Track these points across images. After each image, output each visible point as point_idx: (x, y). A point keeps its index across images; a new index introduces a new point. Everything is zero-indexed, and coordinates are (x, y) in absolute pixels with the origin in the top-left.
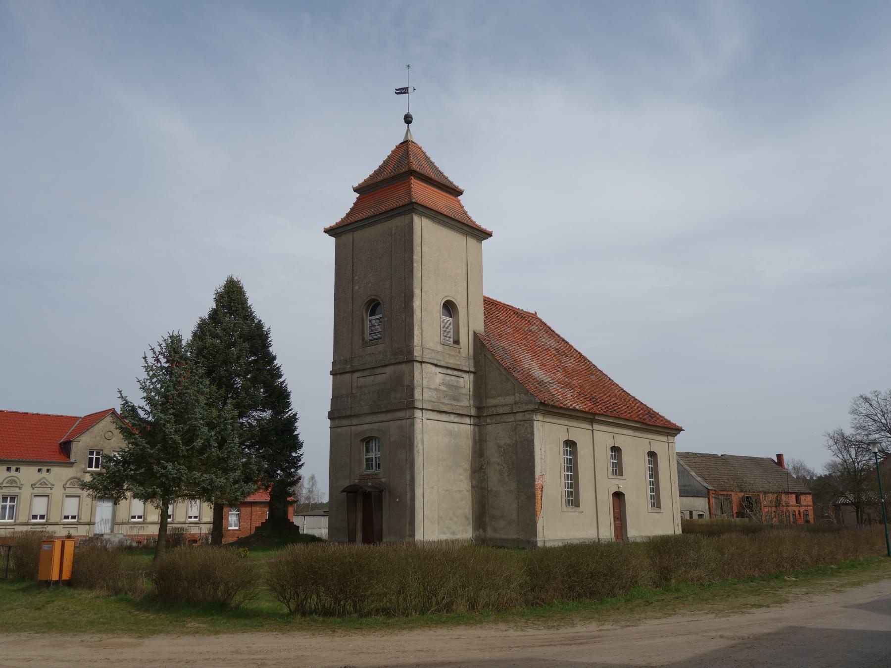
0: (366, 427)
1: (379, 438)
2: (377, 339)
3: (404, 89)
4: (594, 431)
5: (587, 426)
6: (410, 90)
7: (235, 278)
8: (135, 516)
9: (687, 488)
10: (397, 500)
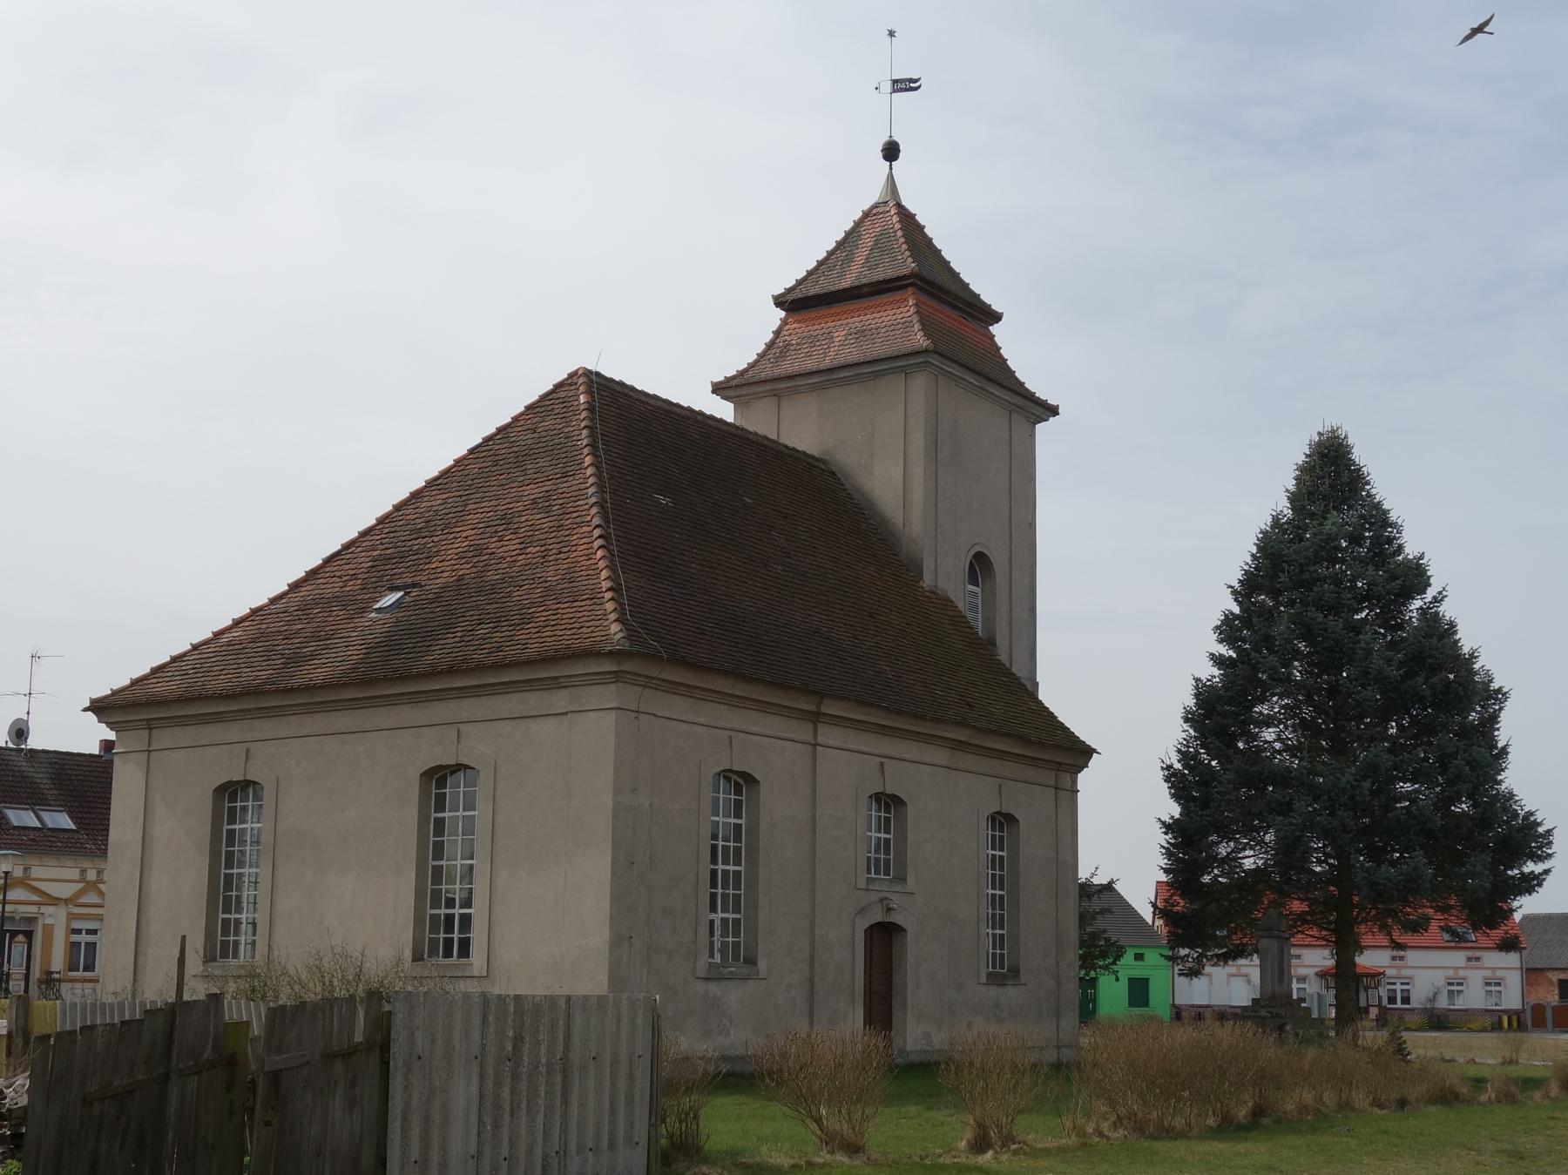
3: (901, 90)
4: (818, 747)
5: (803, 731)
6: (887, 87)
8: (81, 930)
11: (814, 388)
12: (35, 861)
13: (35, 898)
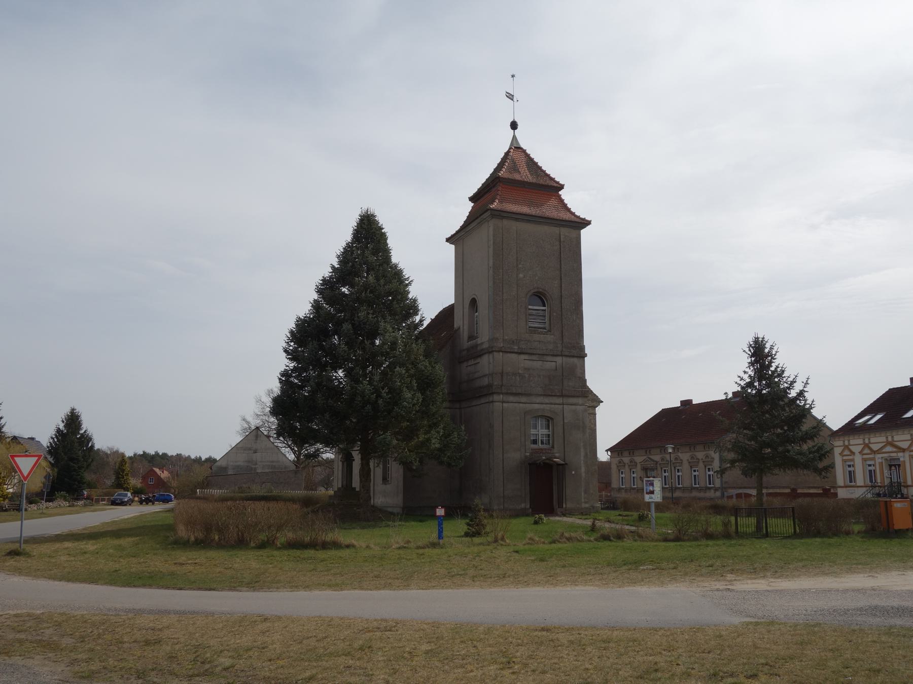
0: (536, 406)
1: (552, 419)
2: (535, 328)
7: (371, 211)
9: (274, 464)
10: (573, 472)
12: (894, 433)
13: (895, 450)
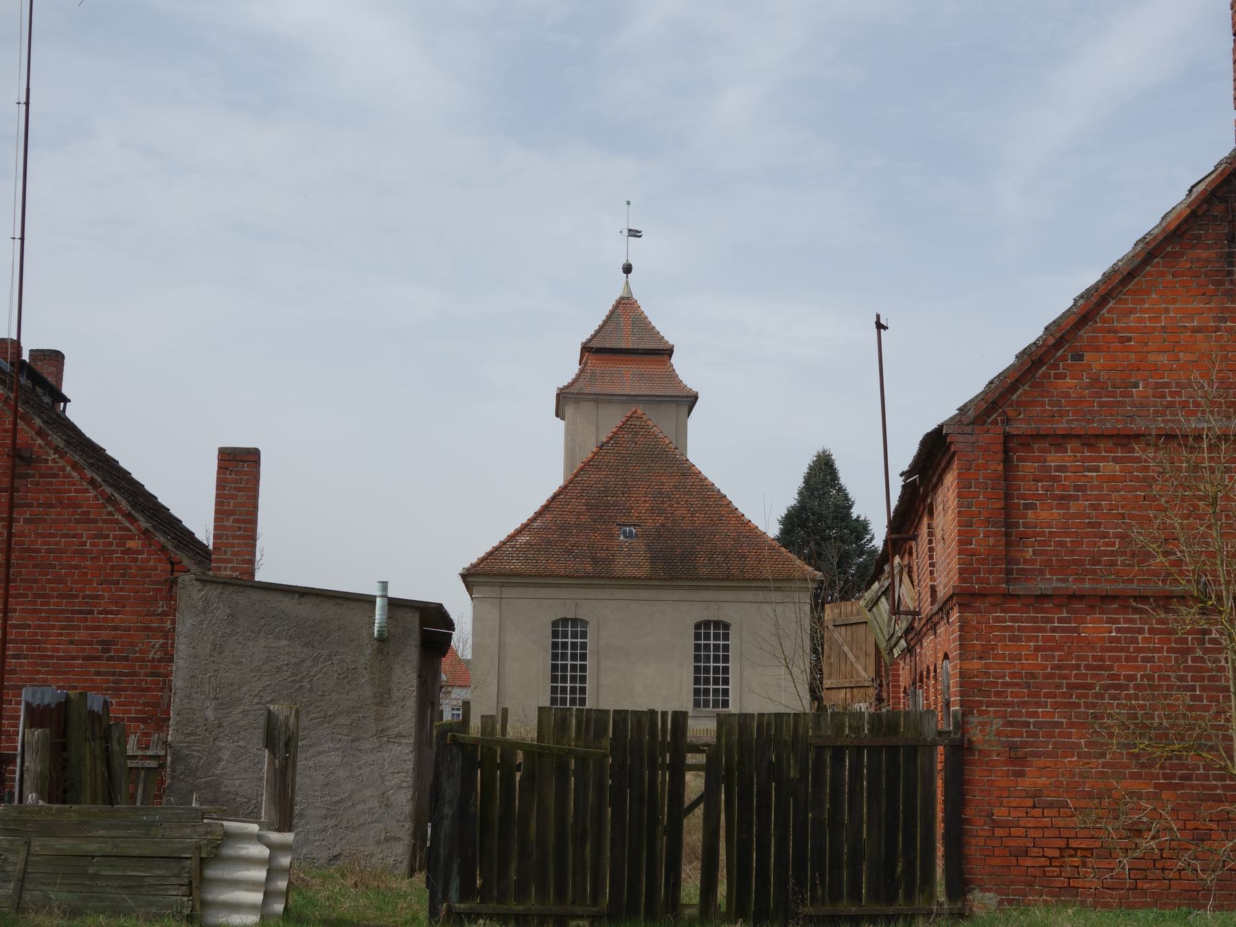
6: (626, 232)
11: (621, 402)
